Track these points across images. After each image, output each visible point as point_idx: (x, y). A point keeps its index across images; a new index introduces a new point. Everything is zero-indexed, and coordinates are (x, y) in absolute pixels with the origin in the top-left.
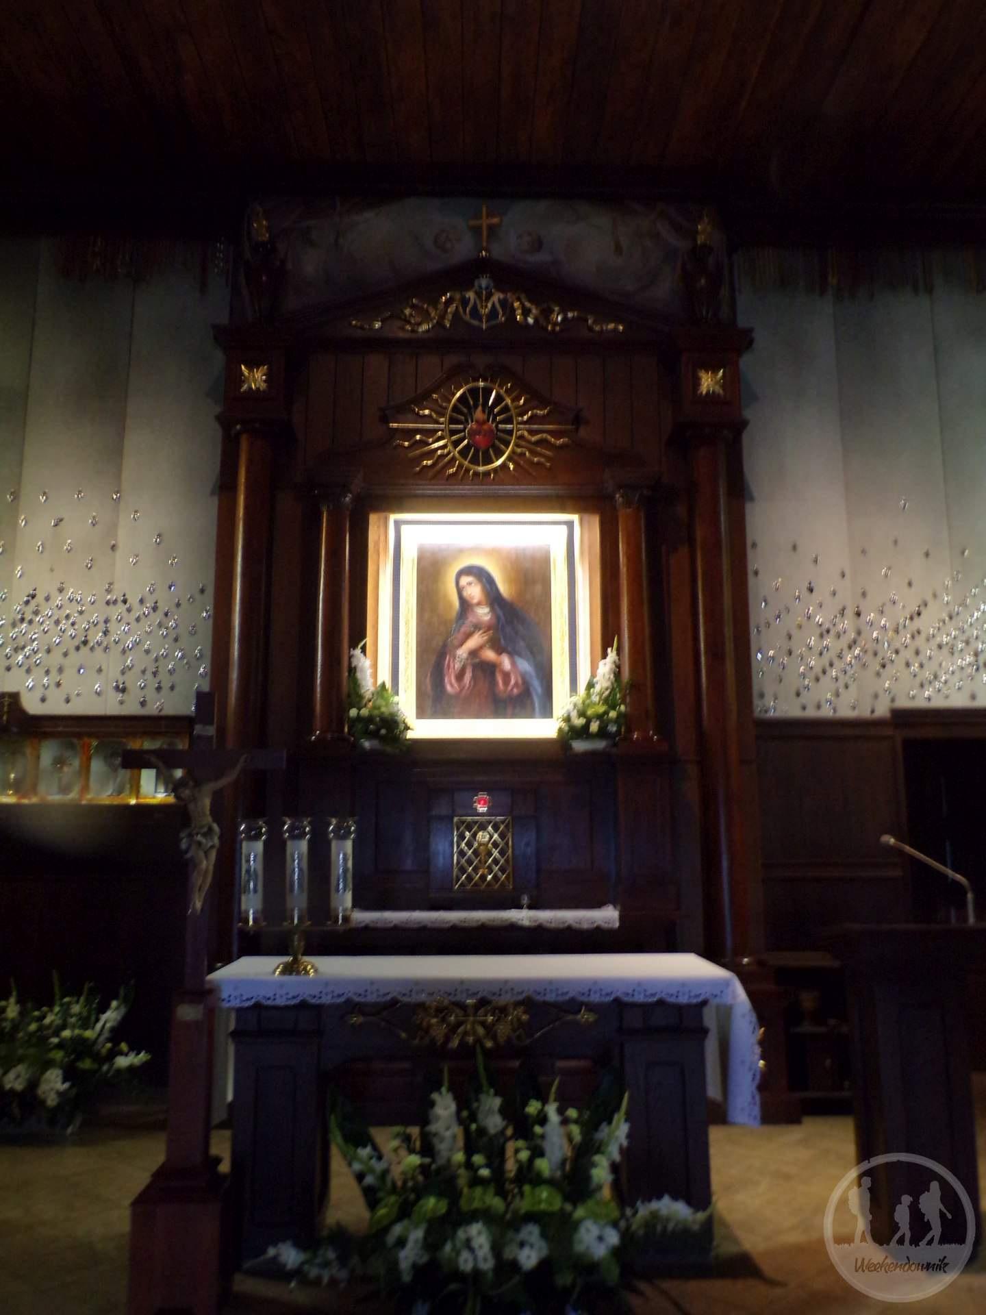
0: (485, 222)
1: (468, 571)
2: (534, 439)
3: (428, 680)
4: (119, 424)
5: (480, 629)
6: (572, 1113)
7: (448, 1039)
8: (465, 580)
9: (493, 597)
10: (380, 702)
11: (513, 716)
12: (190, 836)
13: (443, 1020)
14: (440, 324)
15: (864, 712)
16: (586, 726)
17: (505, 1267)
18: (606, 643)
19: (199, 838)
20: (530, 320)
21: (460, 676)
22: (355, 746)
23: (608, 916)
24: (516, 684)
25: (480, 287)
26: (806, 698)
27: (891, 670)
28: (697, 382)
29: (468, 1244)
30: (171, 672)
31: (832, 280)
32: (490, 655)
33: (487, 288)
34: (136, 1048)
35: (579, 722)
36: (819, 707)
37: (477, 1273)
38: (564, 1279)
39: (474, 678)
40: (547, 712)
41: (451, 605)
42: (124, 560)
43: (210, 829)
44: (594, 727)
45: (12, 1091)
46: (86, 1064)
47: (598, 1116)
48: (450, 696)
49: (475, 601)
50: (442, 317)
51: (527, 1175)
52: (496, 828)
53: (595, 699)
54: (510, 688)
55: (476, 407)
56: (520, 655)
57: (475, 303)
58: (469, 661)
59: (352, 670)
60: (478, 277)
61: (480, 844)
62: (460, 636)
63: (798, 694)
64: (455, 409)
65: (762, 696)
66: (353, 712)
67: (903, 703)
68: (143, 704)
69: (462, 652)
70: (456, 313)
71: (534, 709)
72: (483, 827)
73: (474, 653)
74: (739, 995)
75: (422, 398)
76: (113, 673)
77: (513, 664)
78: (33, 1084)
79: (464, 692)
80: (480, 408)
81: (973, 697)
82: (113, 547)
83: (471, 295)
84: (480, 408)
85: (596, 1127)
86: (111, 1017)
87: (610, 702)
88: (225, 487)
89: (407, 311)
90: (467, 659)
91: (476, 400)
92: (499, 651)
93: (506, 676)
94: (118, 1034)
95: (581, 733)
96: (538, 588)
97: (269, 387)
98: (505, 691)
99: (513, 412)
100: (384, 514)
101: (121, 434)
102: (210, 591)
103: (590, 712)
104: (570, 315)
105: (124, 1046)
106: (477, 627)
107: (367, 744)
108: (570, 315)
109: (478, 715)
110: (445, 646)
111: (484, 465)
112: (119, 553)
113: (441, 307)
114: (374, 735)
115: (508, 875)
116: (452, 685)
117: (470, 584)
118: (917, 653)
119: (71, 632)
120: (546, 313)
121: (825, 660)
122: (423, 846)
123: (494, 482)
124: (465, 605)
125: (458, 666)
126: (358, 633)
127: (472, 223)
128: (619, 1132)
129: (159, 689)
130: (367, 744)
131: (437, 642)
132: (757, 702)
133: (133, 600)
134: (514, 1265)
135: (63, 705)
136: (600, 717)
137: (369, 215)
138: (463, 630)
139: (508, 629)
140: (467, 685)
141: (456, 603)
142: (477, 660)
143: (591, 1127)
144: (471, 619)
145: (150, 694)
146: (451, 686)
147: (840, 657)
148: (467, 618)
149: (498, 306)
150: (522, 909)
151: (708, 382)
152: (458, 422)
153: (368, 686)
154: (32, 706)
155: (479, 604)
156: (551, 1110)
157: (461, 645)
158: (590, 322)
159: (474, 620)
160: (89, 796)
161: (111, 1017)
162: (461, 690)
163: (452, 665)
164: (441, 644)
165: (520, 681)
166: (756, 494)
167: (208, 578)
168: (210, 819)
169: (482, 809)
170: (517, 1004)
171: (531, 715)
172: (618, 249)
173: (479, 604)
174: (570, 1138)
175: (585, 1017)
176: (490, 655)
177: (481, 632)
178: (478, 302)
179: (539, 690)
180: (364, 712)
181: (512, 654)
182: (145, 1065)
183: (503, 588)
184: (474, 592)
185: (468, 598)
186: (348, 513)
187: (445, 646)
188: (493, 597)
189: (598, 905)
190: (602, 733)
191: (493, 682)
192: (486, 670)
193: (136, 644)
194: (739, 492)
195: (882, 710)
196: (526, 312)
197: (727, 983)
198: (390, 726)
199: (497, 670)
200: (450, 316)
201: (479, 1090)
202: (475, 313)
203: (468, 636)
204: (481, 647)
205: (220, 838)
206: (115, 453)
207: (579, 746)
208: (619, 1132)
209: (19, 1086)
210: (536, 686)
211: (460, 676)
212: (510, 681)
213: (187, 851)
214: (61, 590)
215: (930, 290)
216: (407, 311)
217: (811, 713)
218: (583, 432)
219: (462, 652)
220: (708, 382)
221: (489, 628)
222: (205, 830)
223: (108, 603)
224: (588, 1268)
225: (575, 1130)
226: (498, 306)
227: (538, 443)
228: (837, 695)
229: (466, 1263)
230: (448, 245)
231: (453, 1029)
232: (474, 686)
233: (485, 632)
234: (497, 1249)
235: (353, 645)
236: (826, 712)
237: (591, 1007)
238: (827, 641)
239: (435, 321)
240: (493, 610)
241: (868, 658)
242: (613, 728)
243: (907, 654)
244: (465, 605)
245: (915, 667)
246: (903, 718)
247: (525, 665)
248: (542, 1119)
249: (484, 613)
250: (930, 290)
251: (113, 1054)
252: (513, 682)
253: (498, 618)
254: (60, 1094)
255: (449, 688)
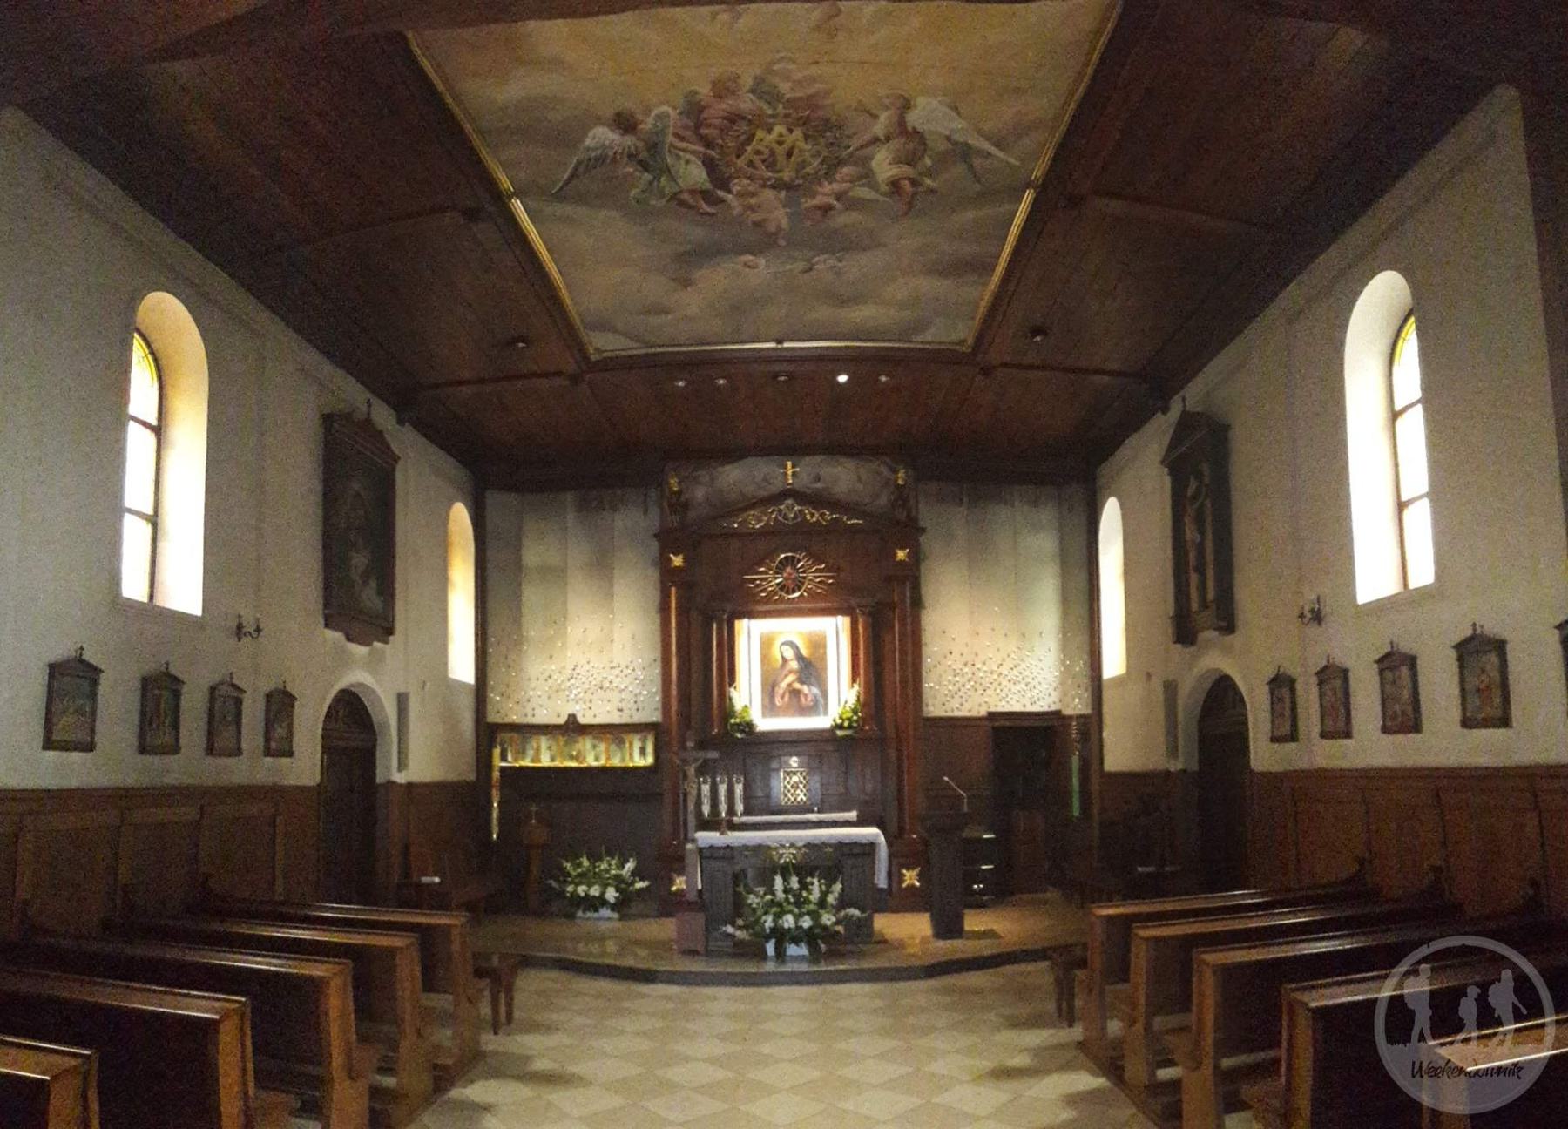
2: (818, 580)
4: (610, 579)
6: (823, 881)
8: (785, 648)
9: (799, 657)
10: (745, 715)
11: (810, 716)
15: (974, 714)
16: (842, 724)
17: (798, 928)
18: (854, 681)
21: (783, 697)
22: (732, 736)
23: (852, 815)
26: (948, 706)
27: (988, 692)
28: (895, 555)
29: (787, 921)
30: (643, 701)
31: (965, 500)
34: (642, 879)
35: (839, 721)
36: (953, 711)
37: (790, 929)
38: (817, 931)
39: (790, 698)
40: (826, 713)
41: (777, 660)
42: (617, 646)
44: (846, 724)
45: (594, 897)
46: (623, 886)
47: (831, 881)
51: (807, 901)
52: (801, 774)
53: (848, 709)
59: (731, 699)
63: (944, 704)
65: (927, 705)
66: (732, 721)
67: (993, 709)
68: (631, 717)
69: (783, 685)
72: (795, 774)
73: (789, 685)
74: (882, 838)
75: (761, 563)
76: (616, 703)
78: (603, 893)
81: (1024, 706)
82: (612, 641)
85: (831, 886)
86: (630, 866)
87: (855, 712)
88: (664, 609)
92: (802, 683)
93: (806, 696)
94: (633, 873)
95: (841, 727)
101: (612, 586)
102: (659, 659)
103: (844, 717)
105: (637, 879)
106: (791, 672)
107: (739, 736)
112: (615, 644)
114: (742, 731)
118: (1000, 684)
119: (594, 683)
121: (956, 688)
122: (768, 785)
123: (797, 603)
124: (785, 660)
125: (781, 691)
126: (732, 681)
128: (838, 887)
129: (638, 710)
130: (739, 736)
132: (925, 709)
133: (623, 666)
134: (801, 927)
136: (849, 719)
141: (780, 661)
143: (829, 886)
144: (788, 668)
145: (634, 711)
146: (778, 702)
147: (964, 686)
150: (370, 1099)
151: (901, 555)
153: (738, 706)
156: (815, 880)
161: (630, 866)
166: (927, 605)
167: (657, 654)
169: (795, 765)
170: (804, 846)
171: (819, 714)
172: (860, 479)
174: (603, 326)
175: (829, 850)
176: (797, 686)
180: (738, 720)
181: (809, 685)
182: (648, 887)
183: (804, 652)
189: (849, 810)
190: (850, 727)
191: (799, 700)
192: (796, 693)
193: (626, 687)
194: (917, 603)
195: (983, 712)
196: (812, 515)
197: (877, 835)
198: (749, 725)
201: (791, 875)
202: (785, 517)
203: (786, 676)
204: (793, 682)
206: (610, 596)
207: (840, 733)
208: (838, 887)
209: (597, 894)
211: (783, 697)
214: (588, 663)
215: (1012, 505)
217: (950, 714)
218: (842, 575)
219: (783, 685)
220: (901, 555)
223: (612, 668)
224: (825, 928)
225: (824, 887)
227: (819, 582)
228: (962, 705)
229: (786, 926)
234: (796, 923)
235: (730, 685)
236: (957, 714)
237: (831, 845)
238: (957, 679)
241: (977, 686)
242: (855, 725)
243: (995, 684)
244: (785, 660)
245: (998, 691)
246: (992, 716)
247: (815, 690)
248: (812, 884)
249: (794, 665)
250: (1012, 505)
251: (633, 883)
254: (616, 898)
255: (778, 704)
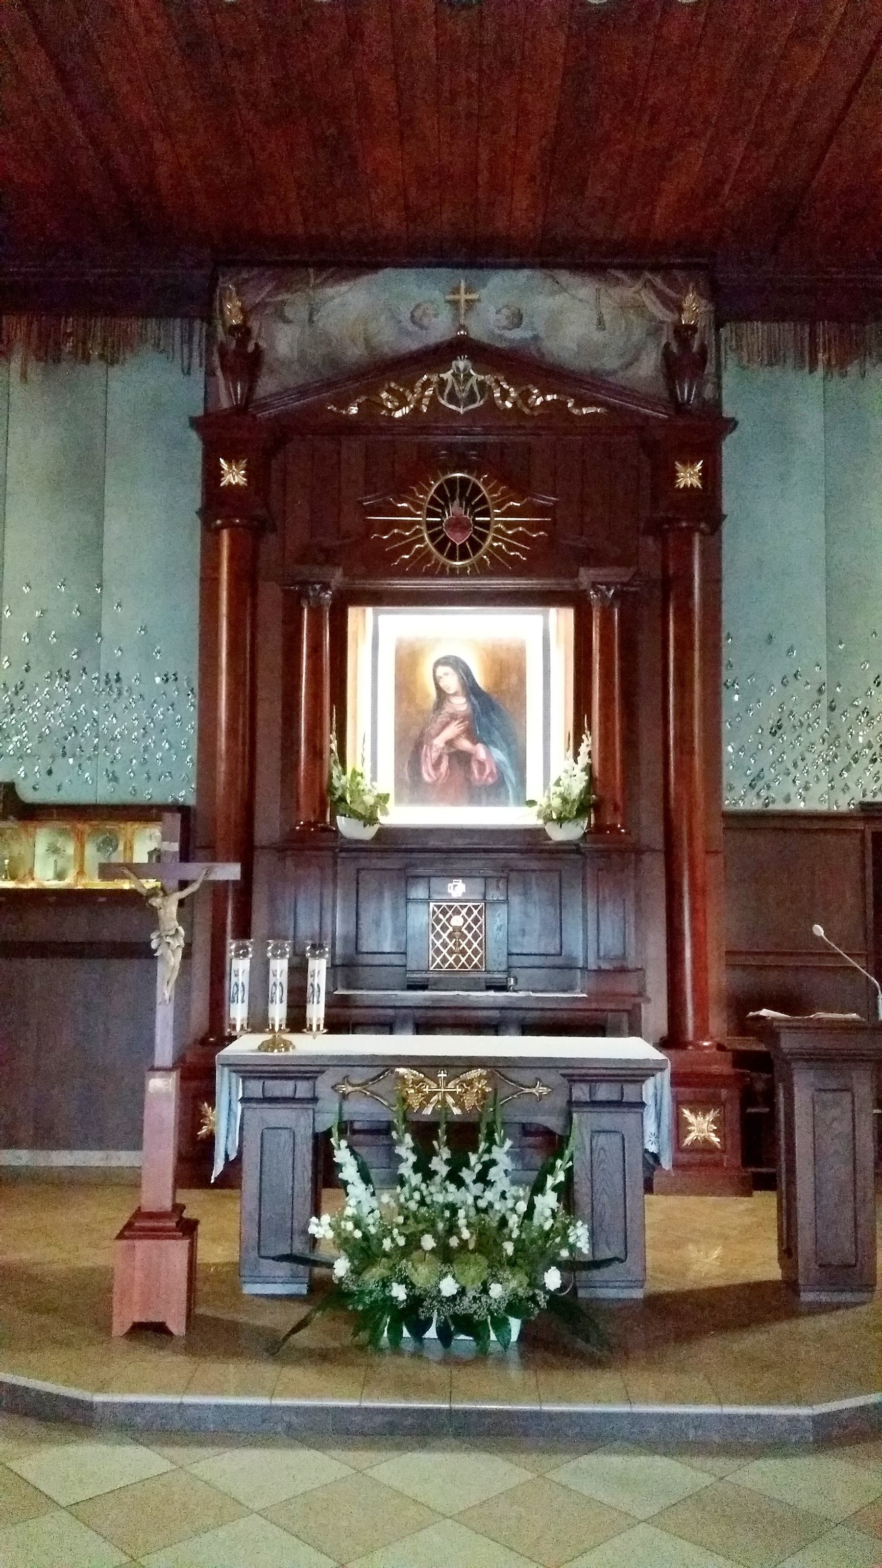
0: (463, 297)
1: (445, 661)
3: (406, 769)
5: (456, 719)
7: (422, 1106)
8: (441, 670)
9: (471, 689)
12: (159, 937)
13: (419, 1091)
14: (416, 410)
19: (168, 940)
20: (509, 405)
21: (436, 765)
24: (491, 773)
25: (458, 368)
32: (465, 744)
33: (465, 370)
36: (787, 799)
39: (450, 767)
41: (428, 696)
43: (177, 930)
48: (427, 784)
49: (451, 692)
50: (419, 401)
54: (485, 777)
55: (453, 499)
56: (496, 746)
57: (453, 386)
58: (446, 751)
60: (456, 359)
61: (455, 928)
62: (436, 726)
64: (433, 501)
69: (439, 742)
70: (433, 399)
71: (508, 797)
73: (450, 743)
77: (489, 753)
79: (440, 782)
80: (457, 502)
83: (447, 376)
84: (457, 502)
89: (384, 395)
90: (443, 749)
91: (453, 492)
92: (475, 740)
93: (481, 764)
96: (514, 679)
97: (248, 482)
98: (480, 780)
99: (490, 504)
100: (363, 608)
104: (549, 398)
106: (453, 717)
108: (549, 398)
109: (455, 802)
110: (422, 734)
111: (461, 560)
113: (418, 390)
115: (481, 958)
116: (429, 775)
117: (446, 674)
120: (525, 395)
124: (442, 696)
125: (435, 755)
127: (450, 297)
131: (415, 732)
135: (56, 793)
137: (344, 287)
138: (439, 720)
139: (484, 720)
140: (444, 774)
142: (453, 750)
144: (448, 709)
146: (427, 774)
148: (444, 709)
149: (476, 389)
152: (436, 515)
154: (28, 795)
155: (455, 694)
157: (438, 735)
158: (570, 405)
159: (451, 711)
160: (84, 882)
162: (438, 779)
163: (429, 754)
164: (418, 733)
165: (495, 771)
168: (177, 923)
172: (601, 324)
173: (455, 694)
176: (465, 744)
177: (457, 722)
178: (456, 385)
179: (513, 779)
183: (480, 680)
184: (451, 682)
185: (445, 689)
186: (327, 609)
187: (422, 734)
188: (471, 689)
191: (469, 770)
192: (461, 759)
196: (505, 395)
199: (473, 759)
200: (426, 401)
204: (458, 736)
205: (185, 939)
210: (510, 773)
211: (436, 765)
212: (485, 770)
213: (156, 951)
216: (384, 395)
219: (439, 742)
221: (465, 718)
222: (173, 932)
226: (476, 389)
230: (425, 321)
231: (428, 1098)
232: (451, 775)
233: (461, 723)
239: (412, 406)
240: (469, 700)
244: (442, 696)
247: (499, 755)
249: (460, 704)
252: (488, 771)
253: (474, 709)
255: (426, 777)
